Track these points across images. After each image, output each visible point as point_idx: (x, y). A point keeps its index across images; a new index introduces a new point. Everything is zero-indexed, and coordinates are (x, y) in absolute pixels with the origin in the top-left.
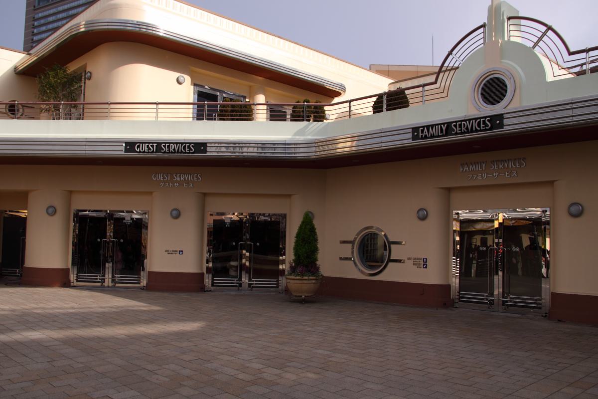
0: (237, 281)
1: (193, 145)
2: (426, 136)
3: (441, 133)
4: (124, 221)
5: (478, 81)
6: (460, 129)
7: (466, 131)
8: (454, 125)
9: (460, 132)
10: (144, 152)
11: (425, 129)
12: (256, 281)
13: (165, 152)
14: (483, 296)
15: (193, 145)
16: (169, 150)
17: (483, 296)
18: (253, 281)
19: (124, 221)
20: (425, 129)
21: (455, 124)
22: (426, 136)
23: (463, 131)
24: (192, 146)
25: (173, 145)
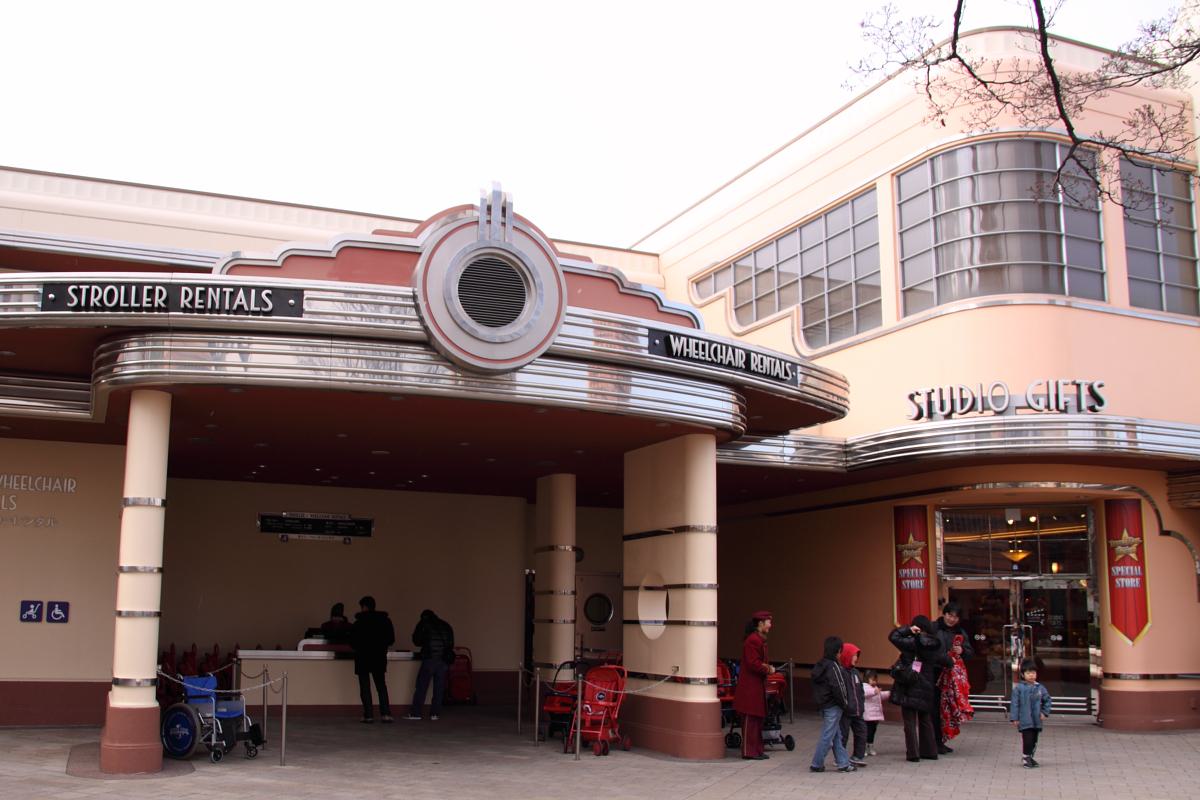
0: (1003, 699)
1: (270, 292)
2: (240, 307)
3: (125, 302)
4: (418, 649)
5: (517, 257)
6: (149, 300)
7: (98, 304)
8: (74, 290)
9: (150, 305)
10: (117, 308)
11: (241, 291)
12: (997, 704)
13: (78, 308)
14: (996, 699)
15: (270, 292)
16: (152, 302)
17: (996, 699)
18: (1003, 705)
19: (418, 649)
20: (241, 291)
21: (75, 287)
22: (240, 307)
23: (156, 305)
24: (267, 295)
25: (100, 290)
